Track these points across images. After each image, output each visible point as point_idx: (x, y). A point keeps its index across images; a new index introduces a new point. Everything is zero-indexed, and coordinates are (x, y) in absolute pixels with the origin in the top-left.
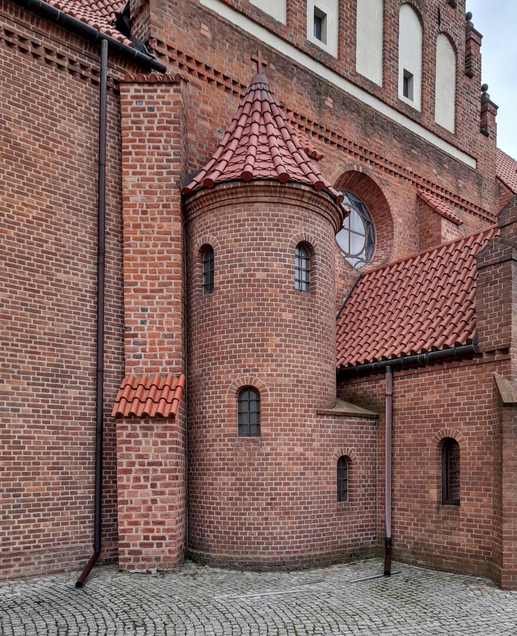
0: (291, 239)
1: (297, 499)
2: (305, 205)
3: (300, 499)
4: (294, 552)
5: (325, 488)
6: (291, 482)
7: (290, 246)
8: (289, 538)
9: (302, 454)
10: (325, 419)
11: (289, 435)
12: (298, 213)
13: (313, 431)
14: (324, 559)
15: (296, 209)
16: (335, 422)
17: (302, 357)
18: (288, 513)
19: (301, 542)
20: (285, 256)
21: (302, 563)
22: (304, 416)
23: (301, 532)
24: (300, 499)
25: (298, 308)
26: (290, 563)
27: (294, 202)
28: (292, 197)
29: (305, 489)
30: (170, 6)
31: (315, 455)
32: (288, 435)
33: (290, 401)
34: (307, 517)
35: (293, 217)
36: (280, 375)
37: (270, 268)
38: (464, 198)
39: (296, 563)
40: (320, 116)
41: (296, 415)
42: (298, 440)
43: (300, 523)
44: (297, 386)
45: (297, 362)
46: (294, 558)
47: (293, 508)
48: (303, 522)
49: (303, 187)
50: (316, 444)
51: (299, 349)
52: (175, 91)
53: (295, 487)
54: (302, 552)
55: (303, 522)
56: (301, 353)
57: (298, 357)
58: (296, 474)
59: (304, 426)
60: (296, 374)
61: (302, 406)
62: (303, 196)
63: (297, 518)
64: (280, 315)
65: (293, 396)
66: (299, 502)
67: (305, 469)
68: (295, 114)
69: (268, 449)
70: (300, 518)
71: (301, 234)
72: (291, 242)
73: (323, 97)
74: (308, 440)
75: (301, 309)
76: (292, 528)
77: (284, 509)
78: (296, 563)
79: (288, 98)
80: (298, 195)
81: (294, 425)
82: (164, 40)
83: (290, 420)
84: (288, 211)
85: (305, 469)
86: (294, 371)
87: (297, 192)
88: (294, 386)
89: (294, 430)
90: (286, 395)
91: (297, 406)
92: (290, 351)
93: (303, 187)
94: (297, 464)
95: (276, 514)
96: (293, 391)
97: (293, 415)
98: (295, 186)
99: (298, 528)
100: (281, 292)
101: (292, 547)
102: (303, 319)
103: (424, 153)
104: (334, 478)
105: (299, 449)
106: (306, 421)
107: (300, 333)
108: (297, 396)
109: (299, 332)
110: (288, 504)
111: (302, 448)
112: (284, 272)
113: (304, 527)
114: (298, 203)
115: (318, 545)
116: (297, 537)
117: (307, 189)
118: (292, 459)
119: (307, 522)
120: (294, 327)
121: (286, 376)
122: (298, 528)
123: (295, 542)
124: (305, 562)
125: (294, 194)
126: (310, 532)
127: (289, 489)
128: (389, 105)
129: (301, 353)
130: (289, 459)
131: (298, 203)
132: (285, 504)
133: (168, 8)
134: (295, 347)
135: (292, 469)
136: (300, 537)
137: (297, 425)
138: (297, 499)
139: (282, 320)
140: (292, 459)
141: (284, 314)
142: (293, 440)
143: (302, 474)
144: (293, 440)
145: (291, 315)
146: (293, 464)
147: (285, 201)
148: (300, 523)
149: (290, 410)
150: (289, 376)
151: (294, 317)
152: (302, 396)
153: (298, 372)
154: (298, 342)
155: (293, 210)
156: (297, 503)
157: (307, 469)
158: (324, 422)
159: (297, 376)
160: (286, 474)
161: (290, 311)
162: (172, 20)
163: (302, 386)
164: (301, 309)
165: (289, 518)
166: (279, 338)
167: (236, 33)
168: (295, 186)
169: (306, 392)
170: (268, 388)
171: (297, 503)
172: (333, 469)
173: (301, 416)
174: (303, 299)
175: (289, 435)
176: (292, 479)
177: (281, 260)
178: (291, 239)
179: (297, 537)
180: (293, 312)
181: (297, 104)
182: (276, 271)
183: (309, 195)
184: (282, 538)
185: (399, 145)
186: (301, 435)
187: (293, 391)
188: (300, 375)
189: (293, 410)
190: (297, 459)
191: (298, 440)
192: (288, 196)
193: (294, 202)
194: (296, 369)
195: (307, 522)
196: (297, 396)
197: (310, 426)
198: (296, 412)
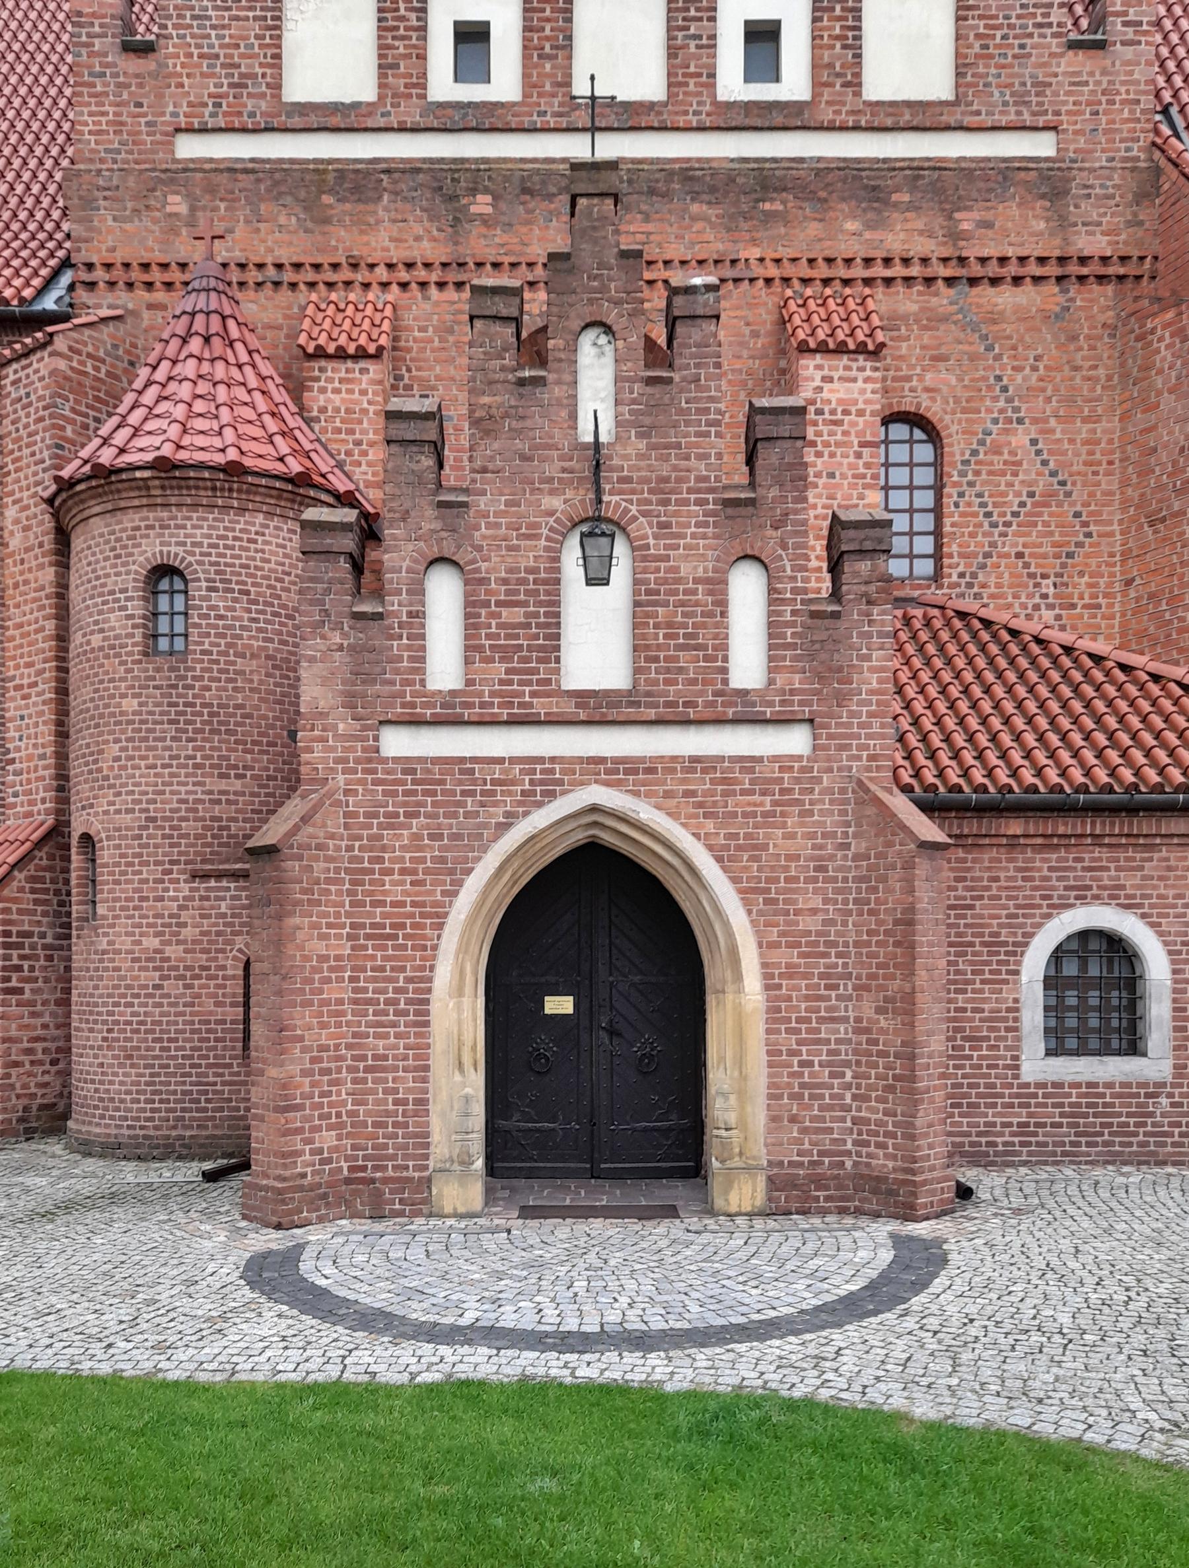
0: (133, 568)
1: (146, 1032)
2: (159, 501)
3: (153, 1031)
4: (142, 1128)
5: (211, 1013)
6: (136, 1001)
7: (135, 580)
8: (133, 1101)
9: (156, 951)
10: (213, 883)
11: (133, 917)
12: (147, 519)
13: (180, 908)
14: (201, 1146)
15: (145, 513)
16: (236, 889)
17: (156, 775)
18: (130, 1057)
19: (153, 1110)
20: (127, 599)
21: (151, 1147)
22: (163, 881)
23: (154, 1093)
24: (153, 1031)
25: (148, 687)
26: (127, 1146)
27: (136, 502)
28: (132, 494)
29: (162, 1014)
30: (105, 198)
31: (186, 951)
32: (132, 917)
33: (135, 855)
34: (168, 1066)
35: (138, 528)
36: (118, 812)
37: (106, 626)
38: (985, 253)
39: (138, 1146)
40: (456, 243)
41: (146, 881)
42: (149, 925)
43: (152, 1075)
44: (147, 828)
45: (147, 784)
46: (136, 1137)
47: (139, 1048)
48: (159, 1075)
49: (138, 474)
50: (188, 933)
51: (151, 761)
52: (51, 355)
53: (142, 1010)
54: (156, 1128)
55: (159, 1075)
56: (154, 767)
57: (148, 775)
58: (146, 987)
59: (162, 899)
60: (144, 806)
61: (156, 863)
62: (148, 488)
63: (146, 1067)
64: (119, 705)
65: (140, 846)
66: (150, 1037)
67: (162, 978)
68: (390, 266)
69: (103, 944)
70: (153, 1066)
71: (154, 554)
72: (136, 572)
73: (464, 201)
74: (170, 925)
75: (155, 687)
76: (138, 1083)
77: (124, 1049)
78: (138, 1146)
79: (367, 244)
80: (139, 488)
81: (142, 899)
82: (95, 259)
83: (135, 891)
84: (131, 519)
85: (162, 978)
86: (140, 802)
87: (133, 484)
88: (140, 828)
89: (141, 908)
90: (128, 847)
91: (147, 863)
92: (134, 767)
93: (138, 474)
94: (146, 969)
95: (114, 1057)
96: (140, 837)
97: (141, 881)
98: (124, 476)
99: (147, 1084)
100: (122, 663)
101: (138, 1119)
102: (157, 705)
103: (812, 197)
104: (234, 995)
105: (152, 943)
106: (167, 890)
107: (153, 731)
108: (147, 846)
109: (149, 731)
110: (130, 1040)
111: (157, 940)
112: (125, 627)
113: (161, 1083)
114: (145, 501)
115: (192, 1119)
116: (147, 1101)
117: (147, 474)
118: (138, 960)
119: (166, 1075)
120: (142, 722)
121: (128, 811)
122: (147, 1084)
123: (144, 1110)
124: (157, 1147)
125: (132, 489)
126: (175, 1092)
127: (133, 1014)
128: (688, 129)
129: (154, 767)
130: (134, 960)
131: (145, 501)
132: (126, 1040)
133: (102, 202)
134: (142, 758)
135: (137, 978)
136: (153, 1102)
137: (146, 899)
138: (146, 1032)
139: (122, 713)
140: (138, 960)
141: (124, 701)
142: (140, 926)
143: (157, 987)
144: (140, 926)
145: (135, 702)
146: (140, 969)
147: (123, 504)
148: (152, 1075)
149: (135, 873)
150: (132, 811)
151: (140, 704)
152: (156, 846)
153: (149, 802)
154: (148, 749)
155: (137, 516)
156: (146, 1040)
157: (168, 977)
158: (207, 889)
159: (147, 810)
160: (128, 987)
161: (135, 696)
162: (110, 218)
163: (156, 828)
164: (155, 687)
165: (132, 1066)
166: (117, 746)
167: (240, 176)
168: (124, 476)
169: (164, 837)
170: (103, 835)
171: (146, 1040)
172: (234, 977)
173: (156, 881)
174: (158, 670)
175: (133, 917)
176: (138, 996)
177: (121, 609)
178: (133, 568)
179: (147, 1101)
180: (139, 695)
181: (392, 245)
182: (113, 629)
183: (157, 482)
184: (122, 1101)
185: (712, 212)
186: (156, 916)
187: (140, 837)
188: (151, 807)
189: (140, 873)
190: (148, 960)
191: (149, 925)
192: (124, 495)
193: (136, 502)
194: (144, 798)
195: (166, 1075)
196: (147, 846)
197: (175, 899)
198: (145, 876)
